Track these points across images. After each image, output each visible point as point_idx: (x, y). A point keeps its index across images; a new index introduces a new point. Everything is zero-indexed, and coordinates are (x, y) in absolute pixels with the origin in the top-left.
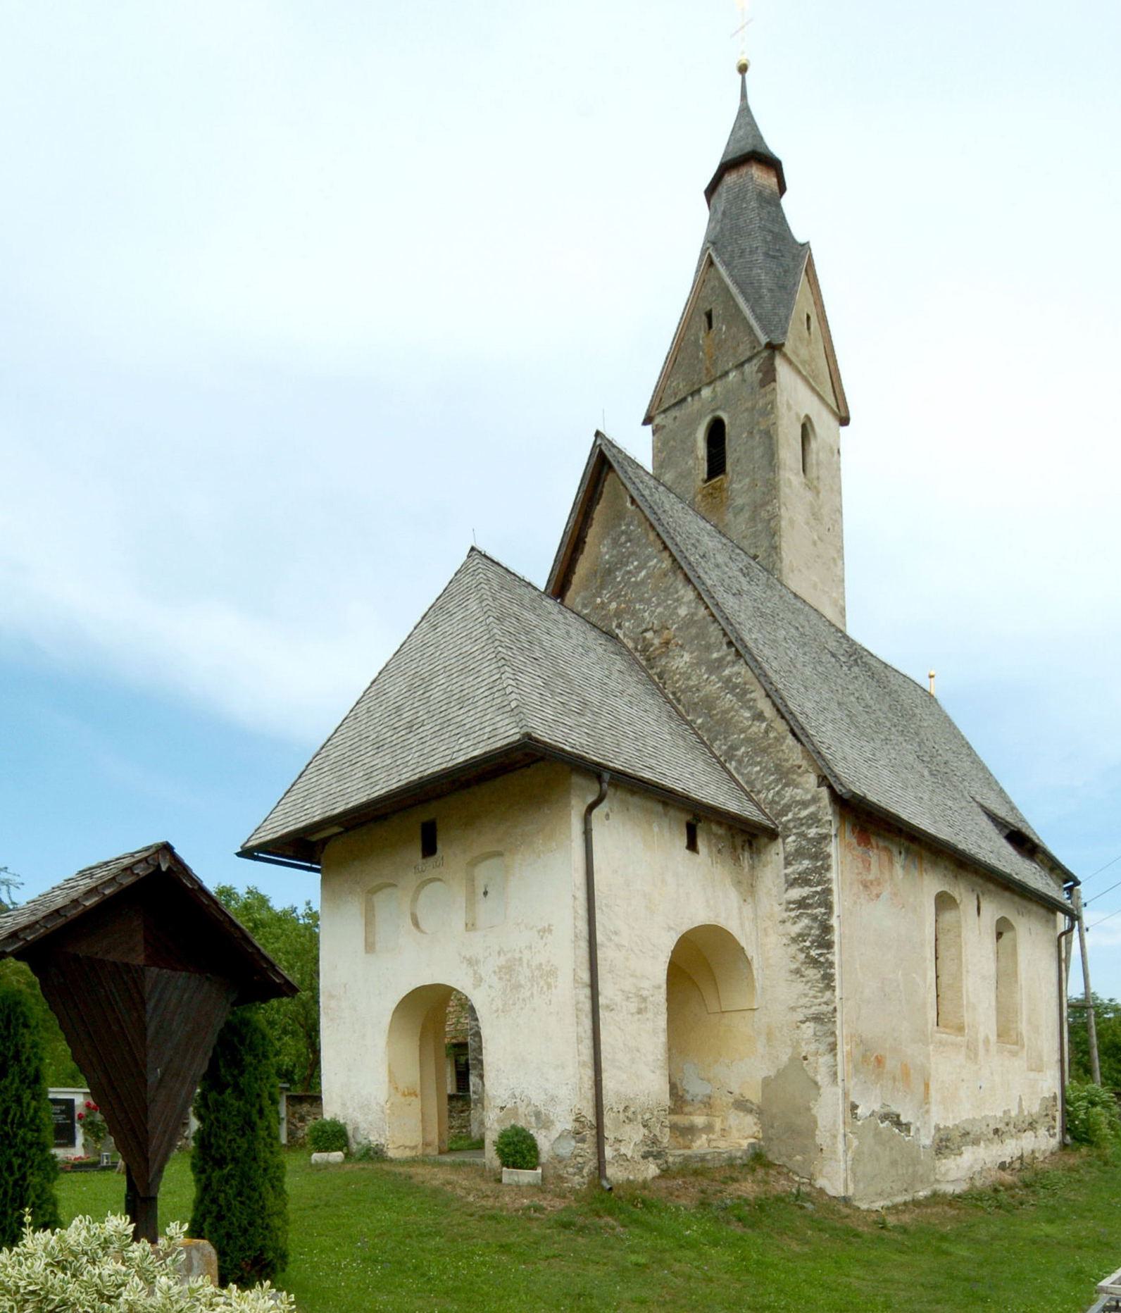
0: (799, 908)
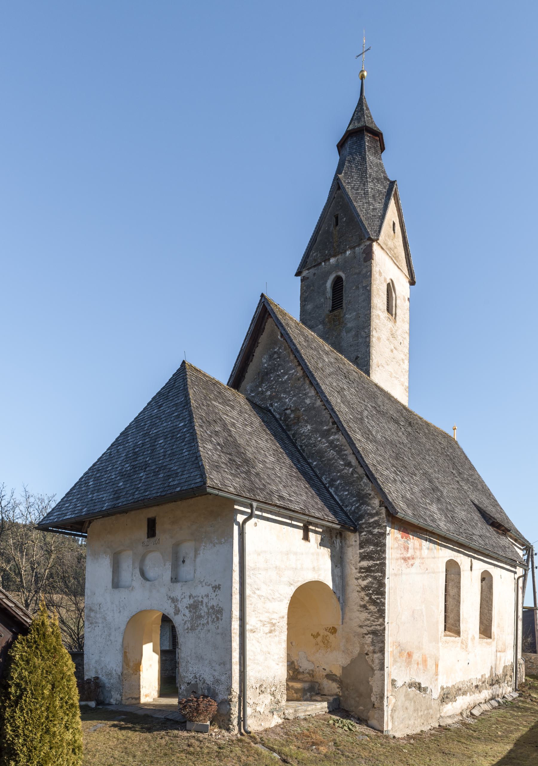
0: (365, 572)
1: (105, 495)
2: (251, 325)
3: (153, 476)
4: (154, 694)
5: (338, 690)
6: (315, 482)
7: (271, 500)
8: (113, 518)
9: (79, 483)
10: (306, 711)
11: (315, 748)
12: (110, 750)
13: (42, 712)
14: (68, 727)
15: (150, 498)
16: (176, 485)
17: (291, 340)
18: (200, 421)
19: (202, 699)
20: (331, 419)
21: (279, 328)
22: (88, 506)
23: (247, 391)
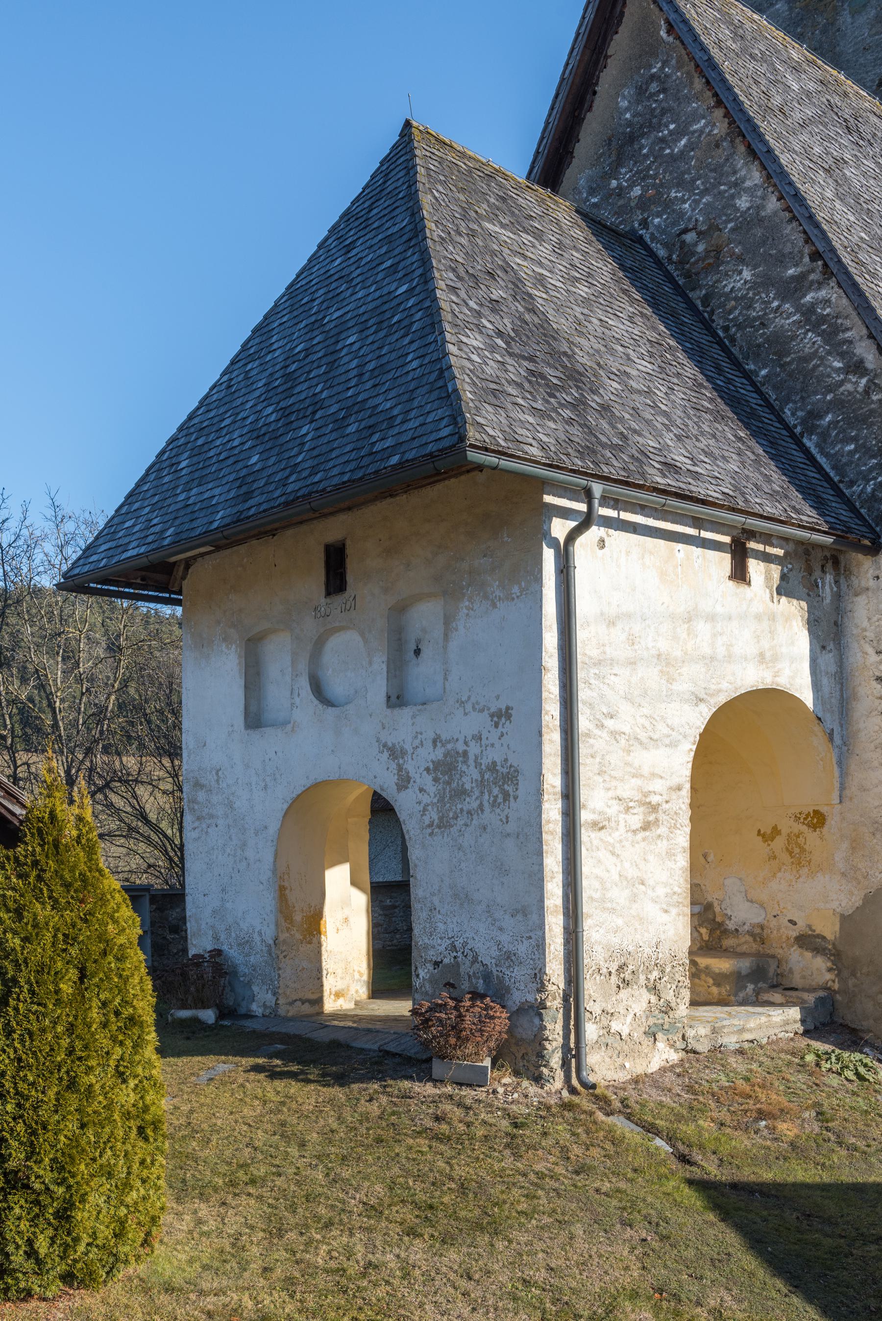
1: (217, 491)
2: (586, 10)
3: (331, 432)
4: (357, 992)
5: (828, 976)
6: (763, 422)
7: (643, 474)
8: (242, 549)
9: (157, 466)
10: (742, 1030)
11: (766, 1127)
12: (245, 1128)
13: (57, 1037)
14: (123, 1073)
15: (324, 489)
16: (389, 450)
17: (696, 38)
18: (451, 275)
19: (468, 1003)
20: (807, 247)
21: (661, 10)
22: (178, 522)
23: (580, 193)
